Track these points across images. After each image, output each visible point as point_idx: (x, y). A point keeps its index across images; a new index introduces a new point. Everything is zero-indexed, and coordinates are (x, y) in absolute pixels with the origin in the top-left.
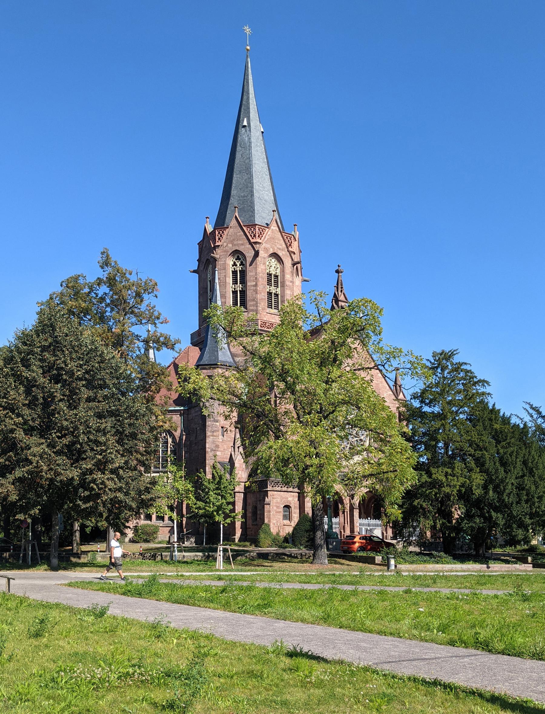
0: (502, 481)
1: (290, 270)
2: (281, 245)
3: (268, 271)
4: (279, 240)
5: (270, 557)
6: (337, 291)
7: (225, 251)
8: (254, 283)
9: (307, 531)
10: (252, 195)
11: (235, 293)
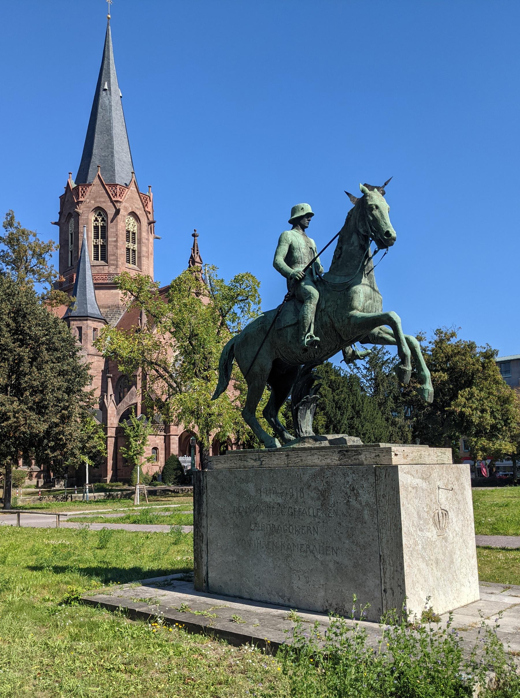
0: (339, 422)
3: (127, 228)
5: (158, 494)
6: (194, 253)
9: (175, 470)
10: (113, 156)
11: (96, 246)
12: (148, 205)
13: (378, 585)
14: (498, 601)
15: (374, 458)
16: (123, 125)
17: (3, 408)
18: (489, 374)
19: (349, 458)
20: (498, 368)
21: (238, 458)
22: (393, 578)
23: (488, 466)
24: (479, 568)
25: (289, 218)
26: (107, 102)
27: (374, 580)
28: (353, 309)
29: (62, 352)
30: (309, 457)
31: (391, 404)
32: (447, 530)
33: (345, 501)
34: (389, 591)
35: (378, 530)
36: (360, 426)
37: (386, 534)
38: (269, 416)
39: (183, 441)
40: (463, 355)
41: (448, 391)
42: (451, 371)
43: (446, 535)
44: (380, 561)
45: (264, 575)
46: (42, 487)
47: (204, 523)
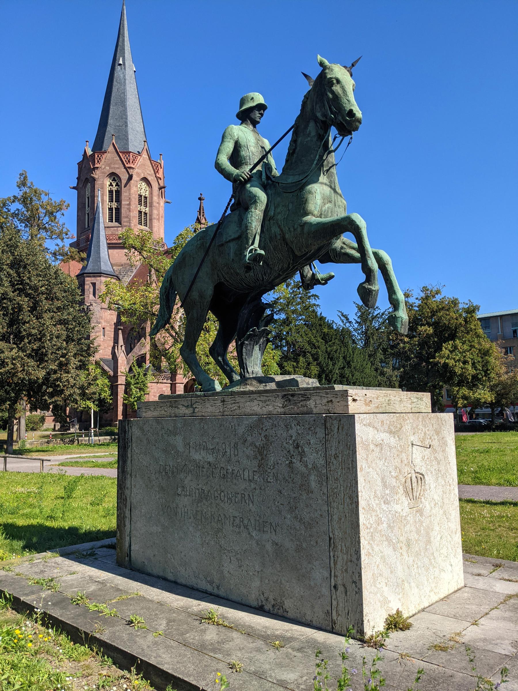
0: (331, 371)
1: (157, 193)
2: (150, 171)
4: (149, 167)
7: (103, 173)
8: (128, 202)
11: (111, 209)
12: (159, 171)
13: (327, 578)
14: (488, 588)
15: (325, 405)
16: (136, 98)
17: (2, 355)
18: (471, 328)
19: (295, 404)
20: (479, 323)
21: (168, 404)
22: (346, 570)
23: (469, 414)
24: (463, 529)
25: (237, 110)
26: (122, 76)
27: (321, 571)
28: (306, 214)
29: (62, 302)
30: (248, 403)
31: (380, 355)
32: (423, 500)
33: (287, 462)
34: (341, 589)
35: (328, 503)
36: (350, 375)
37: (338, 509)
38: (216, 355)
39: (188, 388)
40: (448, 310)
41: (433, 344)
42: (436, 325)
43: (421, 506)
44: (330, 546)
45: (190, 553)
46: (59, 430)
47: (128, 482)
